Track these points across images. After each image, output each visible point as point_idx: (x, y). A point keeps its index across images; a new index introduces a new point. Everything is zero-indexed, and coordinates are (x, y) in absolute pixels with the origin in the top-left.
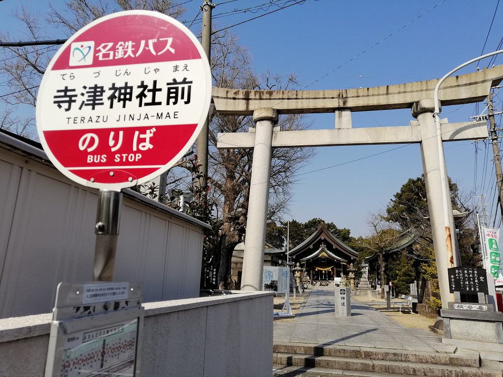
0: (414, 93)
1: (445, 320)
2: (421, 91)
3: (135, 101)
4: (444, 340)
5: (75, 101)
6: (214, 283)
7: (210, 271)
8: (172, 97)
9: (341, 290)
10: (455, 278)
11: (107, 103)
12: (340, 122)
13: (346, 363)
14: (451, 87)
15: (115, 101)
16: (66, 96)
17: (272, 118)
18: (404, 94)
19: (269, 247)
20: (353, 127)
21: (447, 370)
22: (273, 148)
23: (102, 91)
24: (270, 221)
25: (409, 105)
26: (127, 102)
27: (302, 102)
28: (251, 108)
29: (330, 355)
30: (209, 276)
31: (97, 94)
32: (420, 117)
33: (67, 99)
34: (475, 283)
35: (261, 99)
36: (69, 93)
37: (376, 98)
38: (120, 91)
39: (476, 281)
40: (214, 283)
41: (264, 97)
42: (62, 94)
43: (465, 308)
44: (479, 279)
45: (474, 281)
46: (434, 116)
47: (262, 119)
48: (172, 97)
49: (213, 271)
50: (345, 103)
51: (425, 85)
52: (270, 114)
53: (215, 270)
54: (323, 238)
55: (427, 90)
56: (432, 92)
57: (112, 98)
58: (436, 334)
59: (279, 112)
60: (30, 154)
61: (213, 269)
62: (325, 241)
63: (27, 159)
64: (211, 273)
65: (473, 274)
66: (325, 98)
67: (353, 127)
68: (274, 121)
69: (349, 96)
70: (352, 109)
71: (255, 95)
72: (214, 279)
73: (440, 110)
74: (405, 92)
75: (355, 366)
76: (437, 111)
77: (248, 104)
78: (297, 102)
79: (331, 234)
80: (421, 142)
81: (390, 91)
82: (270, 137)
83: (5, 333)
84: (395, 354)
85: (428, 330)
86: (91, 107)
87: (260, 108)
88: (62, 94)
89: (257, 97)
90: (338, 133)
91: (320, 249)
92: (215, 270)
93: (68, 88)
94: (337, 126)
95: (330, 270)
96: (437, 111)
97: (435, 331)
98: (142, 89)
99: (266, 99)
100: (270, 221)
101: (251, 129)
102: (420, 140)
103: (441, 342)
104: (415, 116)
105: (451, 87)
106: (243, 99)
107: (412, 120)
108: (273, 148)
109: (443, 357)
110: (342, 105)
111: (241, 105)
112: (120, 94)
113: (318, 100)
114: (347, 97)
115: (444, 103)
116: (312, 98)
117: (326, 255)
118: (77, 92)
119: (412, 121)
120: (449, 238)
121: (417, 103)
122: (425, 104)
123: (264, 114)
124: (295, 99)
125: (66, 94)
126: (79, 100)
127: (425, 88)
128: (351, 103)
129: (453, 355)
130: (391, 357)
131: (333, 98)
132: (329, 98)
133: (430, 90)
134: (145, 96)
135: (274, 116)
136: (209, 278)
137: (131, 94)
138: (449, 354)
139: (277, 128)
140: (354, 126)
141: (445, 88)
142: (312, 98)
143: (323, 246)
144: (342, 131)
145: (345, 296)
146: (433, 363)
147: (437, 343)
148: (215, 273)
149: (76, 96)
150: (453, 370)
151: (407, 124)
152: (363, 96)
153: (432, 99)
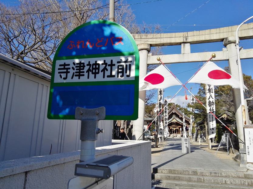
0: (225, 33)
1: (241, 154)
2: (229, 32)
3: (101, 74)
4: (241, 165)
5: (69, 72)
6: (118, 136)
8: (120, 72)
9: (185, 139)
11: (86, 74)
12: (184, 50)
13: (189, 177)
14: (245, 30)
15: (90, 73)
16: (64, 69)
17: (148, 49)
18: (219, 34)
19: (146, 117)
20: (192, 52)
21: (243, 181)
22: (148, 65)
23: (84, 66)
24: (146, 103)
25: (222, 40)
26: (97, 75)
27: (163, 40)
29: (180, 174)
31: (81, 68)
32: (228, 46)
33: (65, 71)
35: (141, 39)
36: (66, 67)
37: (204, 36)
38: (93, 67)
40: (118, 136)
42: (63, 67)
46: (236, 46)
48: (120, 72)
49: (117, 130)
50: (186, 39)
51: (231, 29)
52: (146, 47)
54: (174, 112)
55: (231, 31)
56: (234, 32)
57: (88, 71)
58: (236, 162)
59: (151, 45)
60: (15, 65)
62: (175, 114)
63: (13, 68)
64: (116, 131)
66: (176, 37)
67: (192, 52)
68: (149, 51)
70: (191, 43)
71: (138, 36)
73: (239, 42)
74: (220, 33)
75: (194, 180)
76: (237, 42)
78: (161, 40)
79: (178, 110)
80: (228, 60)
82: (147, 59)
84: (215, 173)
85: (232, 159)
86: (78, 77)
88: (63, 67)
91: (173, 118)
93: (66, 64)
94: (182, 52)
95: (178, 129)
96: (237, 42)
97: (236, 161)
98: (104, 65)
100: (146, 103)
102: (228, 59)
103: (239, 166)
104: (225, 46)
105: (245, 30)
107: (224, 48)
108: (148, 65)
109: (242, 175)
110: (185, 41)
112: (93, 69)
113: (172, 38)
114: (187, 37)
115: (241, 38)
116: (169, 38)
117: (176, 121)
118: (71, 67)
119: (223, 48)
120: (244, 111)
121: (226, 38)
122: (231, 39)
124: (160, 38)
125: (64, 67)
126: (72, 71)
127: (230, 30)
128: (190, 40)
129: (246, 173)
130: (213, 174)
131: (180, 37)
132: (178, 37)
133: (233, 31)
134: (107, 70)
135: (148, 48)
136: (116, 133)
137: (98, 69)
138: (244, 173)
139: (150, 54)
140: (193, 51)
141: (241, 30)
142: (169, 38)
143: (174, 116)
145: (187, 142)
146: (235, 177)
147: (237, 167)
149: (69, 68)
150: (246, 181)
151: (221, 50)
152: (197, 35)
153: (234, 36)
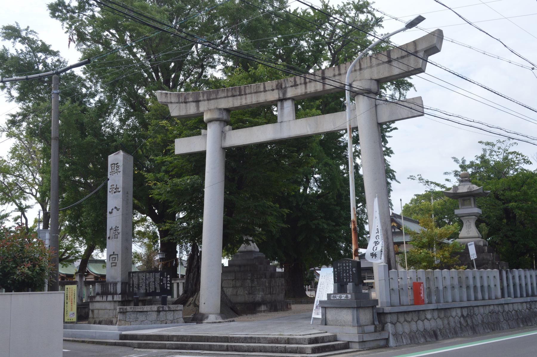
7: (164, 277)
10: (338, 270)
28: (201, 109)
30: (163, 282)
34: (349, 275)
35: (208, 100)
39: (351, 273)
40: (169, 288)
41: (212, 98)
43: (337, 298)
44: (352, 271)
45: (349, 272)
47: (210, 121)
49: (167, 278)
50: (285, 93)
53: (169, 276)
61: (167, 275)
65: (349, 266)
69: (287, 86)
72: (168, 285)
77: (198, 107)
81: (362, 67)
83: (343, 213)
87: (208, 110)
89: (205, 98)
90: (281, 126)
92: (169, 276)
99: (213, 99)
101: (203, 131)
106: (193, 102)
111: (192, 107)
123: (216, 115)
136: (164, 284)
144: (284, 125)
148: (169, 279)
